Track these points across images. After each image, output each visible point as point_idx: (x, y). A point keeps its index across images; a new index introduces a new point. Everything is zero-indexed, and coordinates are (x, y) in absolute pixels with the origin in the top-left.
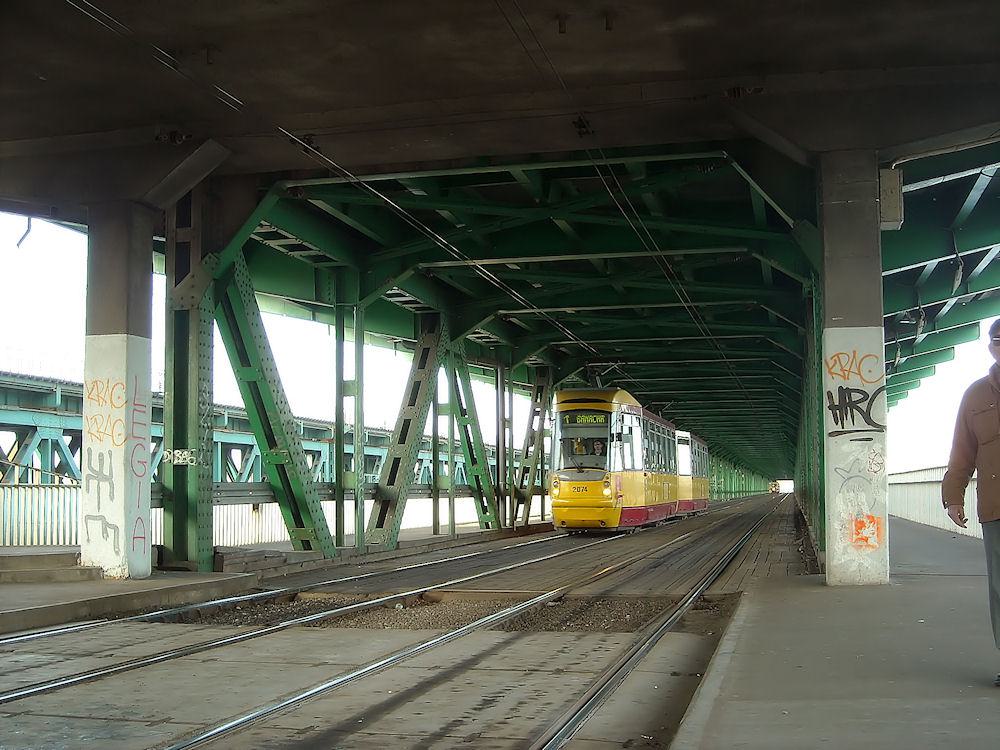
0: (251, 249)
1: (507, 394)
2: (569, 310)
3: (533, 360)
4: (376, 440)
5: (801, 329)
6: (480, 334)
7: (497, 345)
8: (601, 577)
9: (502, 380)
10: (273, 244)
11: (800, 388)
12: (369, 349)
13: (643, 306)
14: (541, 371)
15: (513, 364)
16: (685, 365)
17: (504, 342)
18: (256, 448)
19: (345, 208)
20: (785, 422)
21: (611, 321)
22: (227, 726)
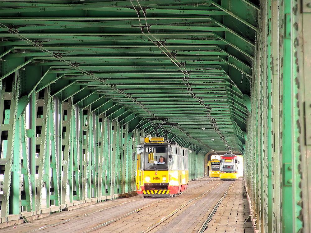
20: (226, 48)
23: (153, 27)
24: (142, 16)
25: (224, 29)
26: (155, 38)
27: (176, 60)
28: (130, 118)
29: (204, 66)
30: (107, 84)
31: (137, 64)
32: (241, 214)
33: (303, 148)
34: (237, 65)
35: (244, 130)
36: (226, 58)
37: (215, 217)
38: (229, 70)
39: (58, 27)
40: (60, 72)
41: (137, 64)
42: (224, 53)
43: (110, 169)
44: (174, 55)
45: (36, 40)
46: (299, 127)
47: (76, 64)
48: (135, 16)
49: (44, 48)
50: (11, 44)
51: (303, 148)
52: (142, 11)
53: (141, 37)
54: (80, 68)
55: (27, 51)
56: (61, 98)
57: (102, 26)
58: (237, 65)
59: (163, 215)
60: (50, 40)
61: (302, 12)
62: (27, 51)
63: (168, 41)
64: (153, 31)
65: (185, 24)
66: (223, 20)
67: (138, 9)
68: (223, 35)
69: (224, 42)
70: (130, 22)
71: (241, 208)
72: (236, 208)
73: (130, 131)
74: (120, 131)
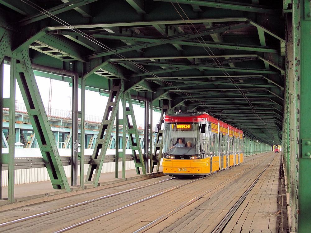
0: (33, 54)
1: (80, 90)
2: (152, 59)
3: (164, 96)
4: (92, 127)
5: (282, 88)
6: (141, 86)
7: (146, 92)
8: (248, 117)
9: (148, 104)
10: (46, 52)
11: (283, 95)
12: (87, 92)
13: (211, 77)
14: (165, 102)
15: (153, 99)
16: (231, 100)
17: (149, 90)
18: (129, 138)
19: (77, 38)
20: (276, 118)
21: (196, 82)
22: (67, 228)
23: (256, 112)
24: (253, 109)
25: (275, 113)
26: (257, 115)
27: (263, 121)
28: (262, 141)
29: (270, 123)
30: (246, 127)
31: (253, 122)
32: (280, 160)
33: (291, 141)
34: (279, 122)
35: (281, 139)
36: (276, 120)
37: (273, 161)
38: (276, 123)
39: (226, 108)
40: (234, 124)
41: (253, 122)
42: (275, 119)
43: (247, 149)
44: (265, 122)
45: (232, 119)
46: (290, 135)
47: (237, 122)
48: (251, 109)
49: (229, 118)
50: (226, 120)
51: (291, 141)
52: (253, 108)
53: (254, 115)
54: (239, 123)
55: (225, 119)
56: (247, 136)
57: (251, 119)
58: (279, 122)
59: (285, 165)
60: (216, 107)
61: (290, 104)
62: (225, 119)
63: (260, 116)
64: (256, 113)
65: (265, 111)
66: (275, 110)
67: (252, 108)
68: (275, 114)
69: (275, 116)
70: (250, 111)
71: (280, 159)
72: (279, 159)
73: (252, 139)
74: (250, 139)
